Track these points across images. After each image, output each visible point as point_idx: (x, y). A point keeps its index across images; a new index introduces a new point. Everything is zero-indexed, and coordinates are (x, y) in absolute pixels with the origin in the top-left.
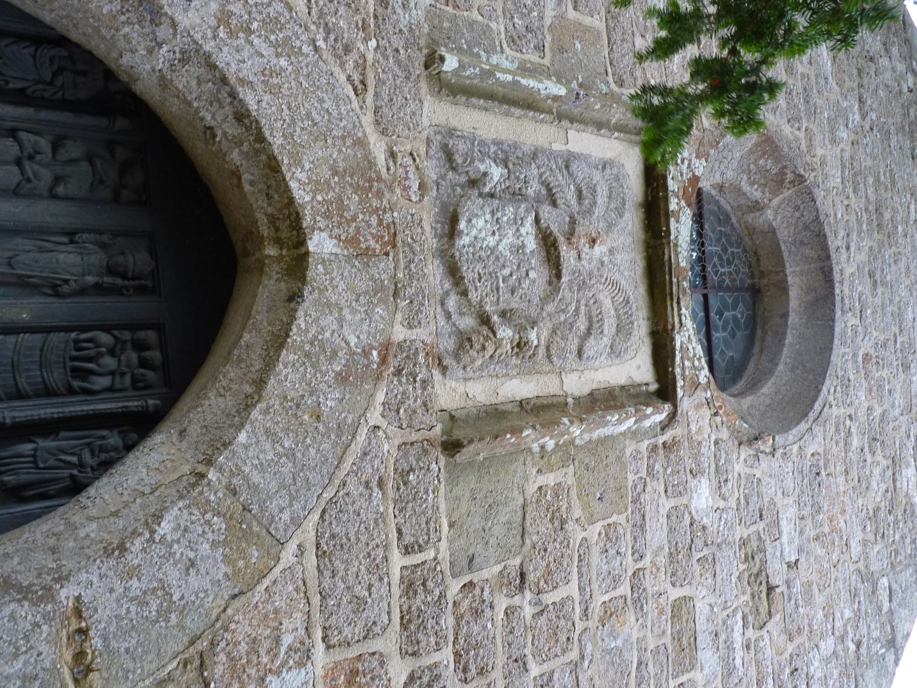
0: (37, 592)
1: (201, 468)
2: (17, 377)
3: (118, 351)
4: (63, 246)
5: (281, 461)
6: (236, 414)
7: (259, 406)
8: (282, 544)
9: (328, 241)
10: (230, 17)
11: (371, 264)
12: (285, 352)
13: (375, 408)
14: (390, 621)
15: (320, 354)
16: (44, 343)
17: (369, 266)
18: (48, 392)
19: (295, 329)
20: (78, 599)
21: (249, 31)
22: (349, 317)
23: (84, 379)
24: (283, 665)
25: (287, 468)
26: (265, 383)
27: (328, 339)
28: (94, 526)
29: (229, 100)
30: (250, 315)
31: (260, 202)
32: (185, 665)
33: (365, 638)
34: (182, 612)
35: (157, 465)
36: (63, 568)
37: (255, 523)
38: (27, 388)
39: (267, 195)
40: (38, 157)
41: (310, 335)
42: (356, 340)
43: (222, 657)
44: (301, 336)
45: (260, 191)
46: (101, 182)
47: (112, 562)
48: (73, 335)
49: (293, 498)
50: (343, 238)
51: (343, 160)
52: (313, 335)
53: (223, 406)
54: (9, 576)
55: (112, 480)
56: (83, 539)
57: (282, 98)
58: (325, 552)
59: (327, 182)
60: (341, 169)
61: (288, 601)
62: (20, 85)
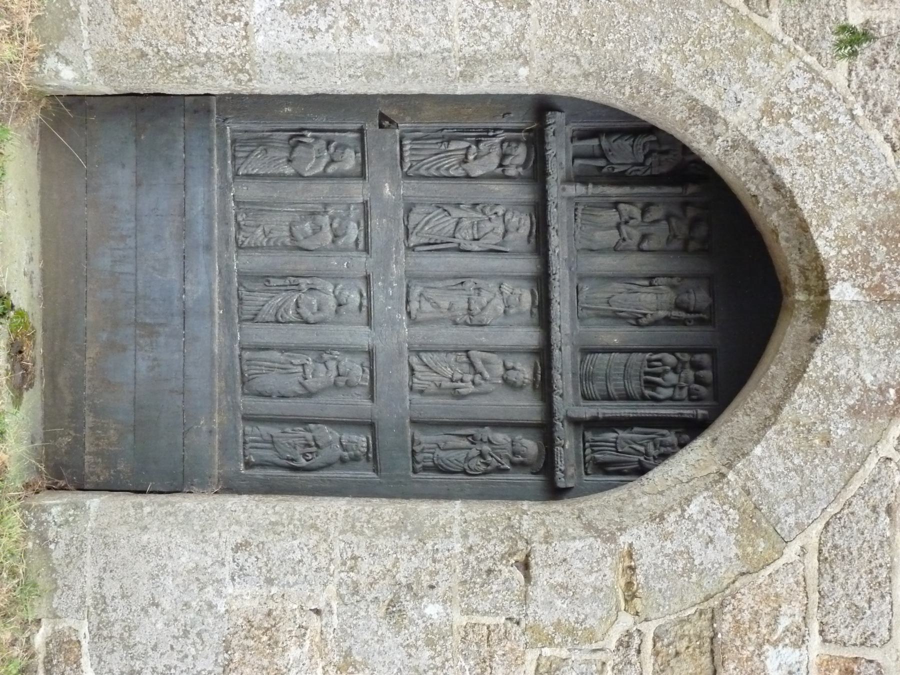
3: (679, 370)
7: (774, 427)
9: (850, 289)
10: (772, 107)
11: (894, 309)
12: (800, 385)
13: (888, 441)
14: (891, 637)
15: (834, 389)
17: (892, 311)
18: (628, 397)
19: (811, 366)
21: (789, 115)
22: (866, 357)
23: (654, 390)
24: (780, 640)
25: (795, 481)
27: (842, 377)
28: (646, 499)
29: (769, 175)
32: (700, 615)
33: (862, 644)
34: (700, 574)
35: (693, 463)
37: (763, 520)
38: (615, 393)
39: (799, 249)
40: (632, 222)
41: (825, 372)
42: (872, 378)
43: (728, 617)
44: (816, 372)
45: (793, 247)
46: (675, 236)
47: (654, 526)
48: (648, 356)
49: (798, 507)
50: (866, 286)
51: (873, 215)
52: (829, 372)
56: (639, 506)
58: (826, 559)
59: (854, 237)
60: (870, 224)
61: (789, 590)
62: (622, 169)
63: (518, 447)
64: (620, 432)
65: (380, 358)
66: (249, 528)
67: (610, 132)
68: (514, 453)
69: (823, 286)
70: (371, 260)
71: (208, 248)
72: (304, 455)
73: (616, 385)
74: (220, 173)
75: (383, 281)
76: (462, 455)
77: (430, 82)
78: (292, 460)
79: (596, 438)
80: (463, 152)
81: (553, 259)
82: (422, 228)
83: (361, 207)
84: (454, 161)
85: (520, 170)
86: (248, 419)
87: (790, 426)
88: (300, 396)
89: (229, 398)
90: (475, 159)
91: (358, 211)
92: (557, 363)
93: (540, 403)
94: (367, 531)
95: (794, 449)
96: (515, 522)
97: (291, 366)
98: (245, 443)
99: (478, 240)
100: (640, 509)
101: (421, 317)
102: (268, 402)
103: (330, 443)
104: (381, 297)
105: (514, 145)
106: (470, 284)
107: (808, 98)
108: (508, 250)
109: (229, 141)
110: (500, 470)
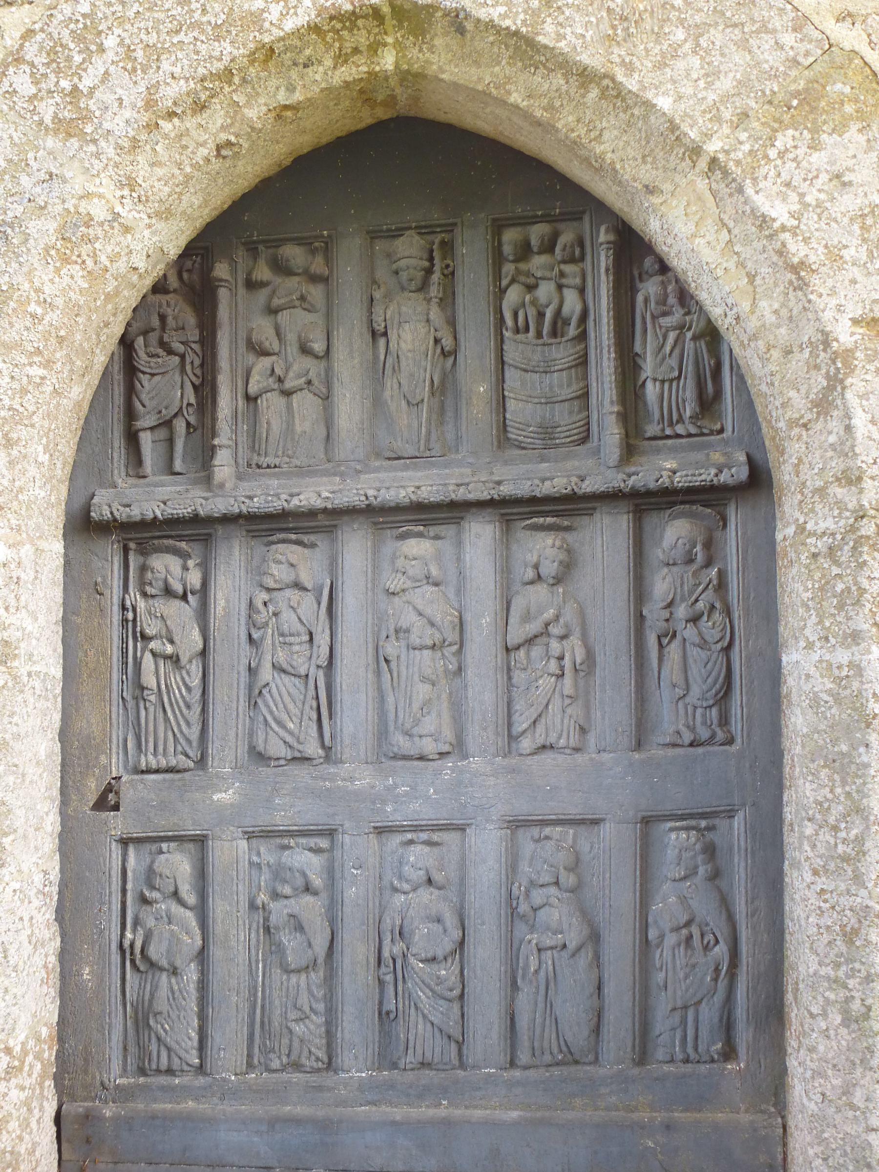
0: (838, 369)
1: (703, 164)
2: (560, 399)
3: (531, 281)
4: (391, 345)
5: (705, 45)
6: (629, 112)
7: (620, 78)
8: (831, 46)
10: (60, 120)
12: (540, 38)
16: (516, 368)
18: (583, 362)
19: (507, 23)
20: (855, 322)
23: (567, 322)
26: (585, 69)
28: (763, 304)
30: (484, 92)
31: (318, 77)
36: (813, 340)
38: (575, 387)
39: (306, 66)
40: (278, 371)
44: (517, 13)
48: (507, 334)
49: (764, 28)
53: (616, 132)
54: (812, 402)
55: (705, 286)
57: (163, 43)
63: (679, 554)
64: (643, 376)
65: (523, 807)
66: (859, 1071)
67: (130, 414)
68: (690, 561)
69: (365, 17)
70: (347, 825)
71: (325, 1126)
72: (706, 948)
73: (561, 386)
74: (196, 1099)
75: (384, 802)
76: (694, 653)
77: (15, 719)
78: (717, 970)
79: (657, 415)
80: (161, 663)
81: (343, 500)
82: (291, 733)
83: (254, 841)
84: (175, 680)
85: (191, 563)
86: (642, 1057)
87: (616, 50)
88: (597, 956)
89: (603, 1090)
90: (172, 642)
91: (262, 850)
92: (523, 489)
93: (597, 516)
94: (855, 832)
95: (657, 42)
96: (821, 545)
97: (542, 974)
98: (687, 1061)
99: (311, 634)
100: (784, 312)
101: (448, 734)
102: (610, 1017)
103: (683, 900)
104: (415, 806)
105: (149, 575)
106: (391, 649)
107: (48, 65)
108: (328, 582)
109: (142, 1080)
110: (722, 585)
